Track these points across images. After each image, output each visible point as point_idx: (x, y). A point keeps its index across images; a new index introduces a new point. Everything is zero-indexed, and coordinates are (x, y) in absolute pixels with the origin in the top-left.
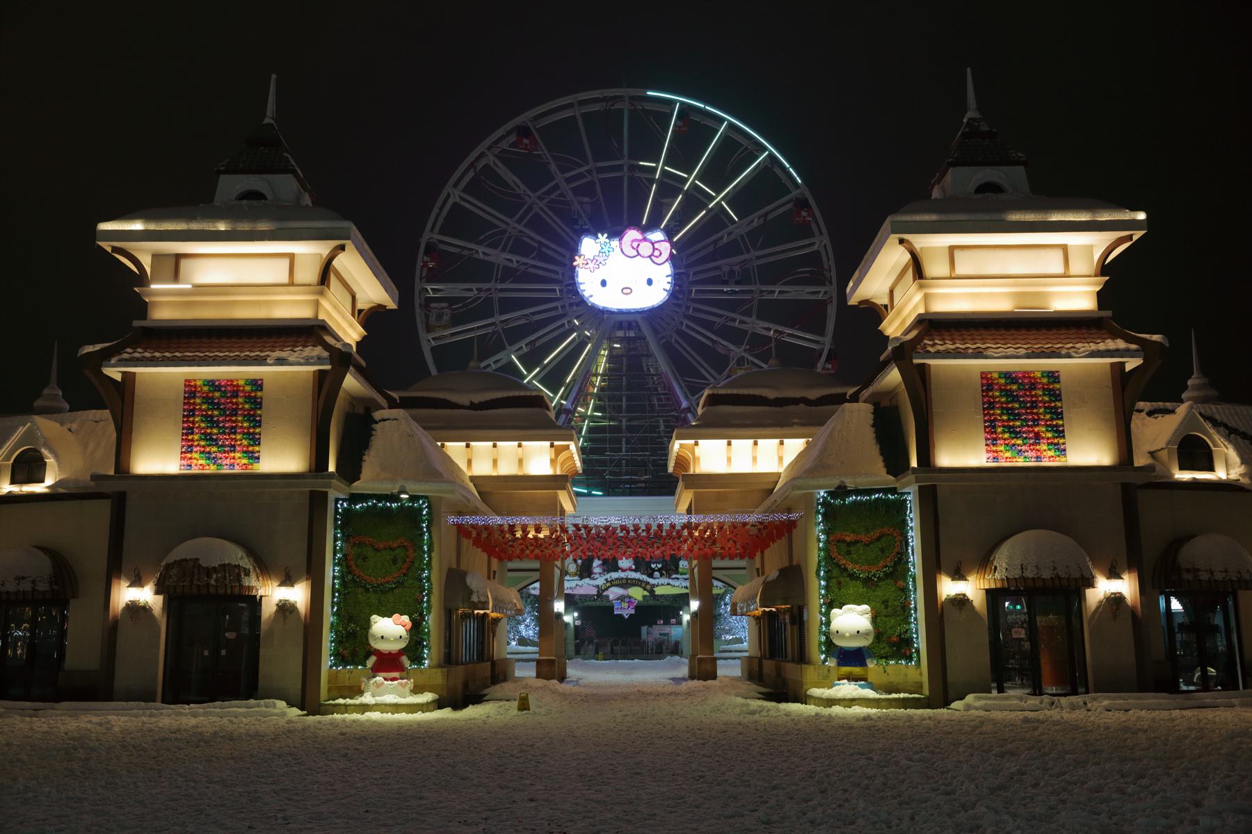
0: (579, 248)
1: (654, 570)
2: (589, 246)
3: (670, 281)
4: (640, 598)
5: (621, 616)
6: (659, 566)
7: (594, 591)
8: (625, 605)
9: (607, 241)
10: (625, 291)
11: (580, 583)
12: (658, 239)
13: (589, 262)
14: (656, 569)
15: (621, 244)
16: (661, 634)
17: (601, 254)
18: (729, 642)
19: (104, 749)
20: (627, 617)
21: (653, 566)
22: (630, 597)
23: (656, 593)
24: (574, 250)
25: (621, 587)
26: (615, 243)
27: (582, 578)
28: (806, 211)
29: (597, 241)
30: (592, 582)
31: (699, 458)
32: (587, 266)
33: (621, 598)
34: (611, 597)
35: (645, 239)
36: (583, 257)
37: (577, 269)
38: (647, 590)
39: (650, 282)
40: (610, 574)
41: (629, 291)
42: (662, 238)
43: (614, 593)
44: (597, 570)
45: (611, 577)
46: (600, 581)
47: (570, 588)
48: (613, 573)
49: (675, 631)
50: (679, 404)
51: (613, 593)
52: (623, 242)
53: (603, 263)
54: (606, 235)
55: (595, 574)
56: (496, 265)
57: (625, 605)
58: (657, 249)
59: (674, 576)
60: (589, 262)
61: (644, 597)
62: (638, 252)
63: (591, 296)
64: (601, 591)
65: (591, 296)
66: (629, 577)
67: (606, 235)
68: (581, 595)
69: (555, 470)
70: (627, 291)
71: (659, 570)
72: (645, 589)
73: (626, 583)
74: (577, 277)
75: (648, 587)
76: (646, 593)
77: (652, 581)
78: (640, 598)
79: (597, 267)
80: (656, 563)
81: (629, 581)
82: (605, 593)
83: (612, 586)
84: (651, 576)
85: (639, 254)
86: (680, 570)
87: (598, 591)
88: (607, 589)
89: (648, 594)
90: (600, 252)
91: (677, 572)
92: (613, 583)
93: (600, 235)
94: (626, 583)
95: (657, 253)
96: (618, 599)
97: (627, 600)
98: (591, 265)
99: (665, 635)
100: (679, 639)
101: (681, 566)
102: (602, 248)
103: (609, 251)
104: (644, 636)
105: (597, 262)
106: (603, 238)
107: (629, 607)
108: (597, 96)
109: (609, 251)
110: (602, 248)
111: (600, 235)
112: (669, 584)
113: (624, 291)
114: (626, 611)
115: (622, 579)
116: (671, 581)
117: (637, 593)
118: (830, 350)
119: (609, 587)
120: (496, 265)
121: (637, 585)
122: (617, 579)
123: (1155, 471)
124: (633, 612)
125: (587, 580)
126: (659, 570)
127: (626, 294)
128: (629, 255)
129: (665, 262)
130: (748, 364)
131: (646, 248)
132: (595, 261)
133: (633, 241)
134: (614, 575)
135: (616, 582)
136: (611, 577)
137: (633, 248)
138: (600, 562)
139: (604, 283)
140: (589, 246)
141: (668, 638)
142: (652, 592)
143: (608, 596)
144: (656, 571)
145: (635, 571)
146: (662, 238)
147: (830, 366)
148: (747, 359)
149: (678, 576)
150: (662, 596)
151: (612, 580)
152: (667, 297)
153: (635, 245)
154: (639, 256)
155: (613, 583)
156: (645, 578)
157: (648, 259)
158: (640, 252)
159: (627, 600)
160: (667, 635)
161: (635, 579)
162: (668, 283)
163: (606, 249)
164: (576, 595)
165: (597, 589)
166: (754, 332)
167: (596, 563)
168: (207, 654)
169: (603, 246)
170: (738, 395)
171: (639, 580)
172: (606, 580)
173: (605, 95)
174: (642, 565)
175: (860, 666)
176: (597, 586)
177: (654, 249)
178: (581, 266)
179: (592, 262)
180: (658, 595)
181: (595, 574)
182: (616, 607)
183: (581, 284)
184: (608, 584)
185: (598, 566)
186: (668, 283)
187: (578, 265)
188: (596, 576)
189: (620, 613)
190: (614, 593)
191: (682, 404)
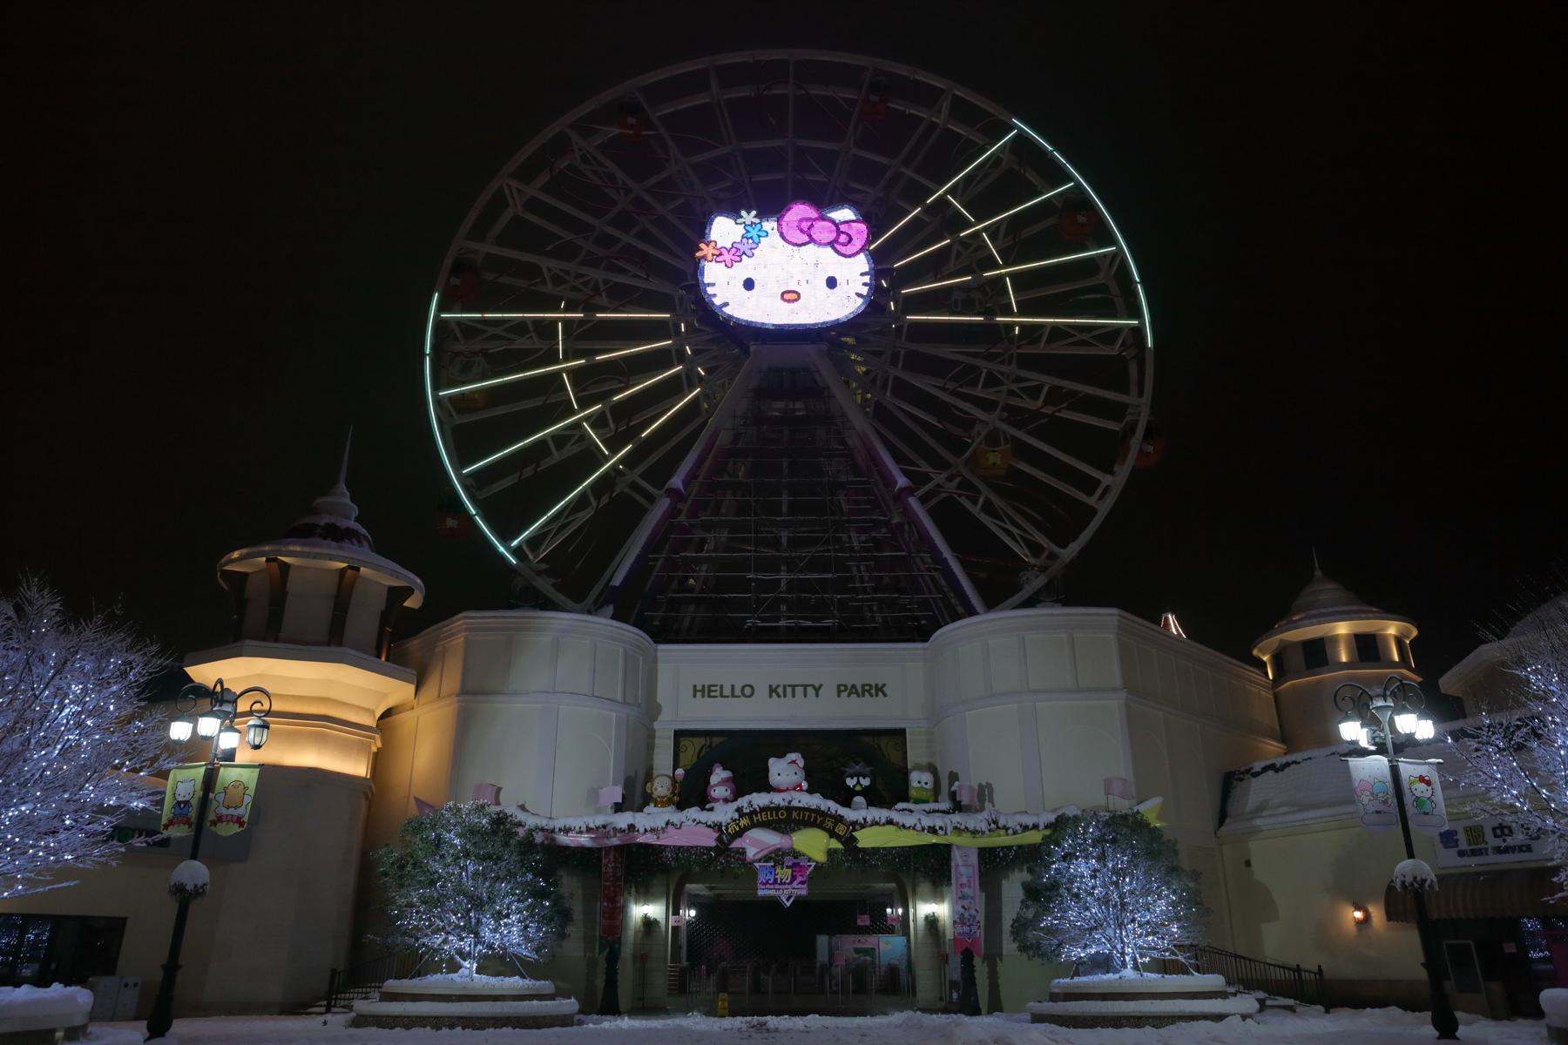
0: (707, 231)
1: (852, 793)
2: (724, 230)
3: (865, 293)
4: (821, 857)
5: (774, 903)
6: (866, 782)
7: (709, 839)
8: (784, 873)
9: (757, 221)
10: (787, 296)
11: (677, 817)
12: (846, 219)
13: (724, 251)
14: (858, 788)
15: (779, 225)
16: (858, 951)
17: (745, 240)
18: (1079, 968)
20: (788, 904)
21: (851, 782)
22: (796, 854)
23: (860, 845)
24: (701, 230)
25: (775, 829)
26: (770, 225)
27: (681, 807)
28: (1083, 216)
29: (739, 221)
30: (704, 816)
32: (720, 259)
33: (776, 857)
34: (751, 853)
35: (823, 218)
36: (713, 244)
37: (703, 263)
38: (838, 837)
39: (832, 283)
40: (747, 798)
41: (792, 296)
42: (853, 217)
44: (719, 792)
45: (750, 804)
46: (724, 814)
47: (653, 830)
48: (755, 794)
49: (887, 943)
50: (889, 481)
51: (755, 843)
52: (784, 224)
53: (749, 253)
54: (754, 213)
55: (716, 800)
57: (784, 873)
58: (843, 233)
59: (900, 805)
60: (724, 251)
61: (831, 853)
62: (810, 236)
63: (726, 304)
64: (726, 837)
65: (726, 304)
66: (795, 804)
67: (754, 213)
68: (679, 849)
70: (791, 296)
71: (865, 792)
72: (832, 834)
73: (787, 820)
74: (703, 275)
75: (841, 829)
77: (849, 814)
78: (821, 857)
79: (739, 259)
80: (858, 776)
81: (794, 814)
82: (736, 844)
83: (753, 825)
84: (847, 803)
85: (812, 240)
86: (913, 793)
87: (719, 839)
88: (740, 833)
89: (839, 846)
90: (743, 237)
91: (906, 799)
92: (758, 819)
93: (743, 213)
94: (787, 820)
95: (843, 238)
96: (767, 859)
97: (789, 861)
98: (727, 256)
99: (866, 952)
100: (896, 962)
101: (914, 784)
102: (748, 232)
103: (759, 236)
104: (822, 954)
105: (737, 253)
106: (749, 217)
107: (794, 878)
108: (744, 60)
109: (759, 236)
110: (748, 232)
111: (743, 213)
112: (890, 822)
113: (786, 296)
114: (786, 890)
115: (778, 808)
116: (895, 816)
117: (813, 844)
118: (1149, 423)
119: (746, 829)
121: (821, 827)
122: (763, 809)
125: (694, 813)
126: (865, 792)
127: (789, 301)
128: (794, 241)
129: (857, 253)
130: (1005, 444)
131: (823, 231)
132: (734, 250)
133: (801, 220)
134: (759, 799)
135: (763, 817)
136: (750, 804)
137: (802, 231)
138: (726, 774)
139: (749, 284)
140: (724, 230)
141: (873, 957)
142: (850, 842)
143: (743, 852)
144: (859, 793)
145: (810, 791)
146: (853, 217)
147: (1150, 449)
148: (1004, 433)
149: (910, 806)
150: (875, 851)
151: (754, 812)
152: (863, 308)
153: (805, 225)
154: (811, 246)
155: (758, 819)
156: (831, 806)
157: (829, 250)
158: (814, 236)
159: (789, 861)
160: (870, 952)
161: (808, 809)
162: (865, 284)
163: (754, 233)
164: (666, 847)
165: (717, 835)
166: (1008, 404)
167: (719, 775)
168: (1507, 950)
169: (749, 228)
170: (961, 588)
171: (818, 811)
172: (739, 810)
173: (758, 58)
174: (824, 778)
175: (1054, 993)
176: (717, 827)
177: (839, 232)
178: (710, 257)
179: (729, 252)
180: (864, 850)
181: (716, 800)
182: (761, 878)
183: (709, 285)
184: (744, 822)
185: (723, 782)
186: (865, 284)
187: (704, 257)
188: (717, 806)
189: (772, 892)
191: (896, 483)
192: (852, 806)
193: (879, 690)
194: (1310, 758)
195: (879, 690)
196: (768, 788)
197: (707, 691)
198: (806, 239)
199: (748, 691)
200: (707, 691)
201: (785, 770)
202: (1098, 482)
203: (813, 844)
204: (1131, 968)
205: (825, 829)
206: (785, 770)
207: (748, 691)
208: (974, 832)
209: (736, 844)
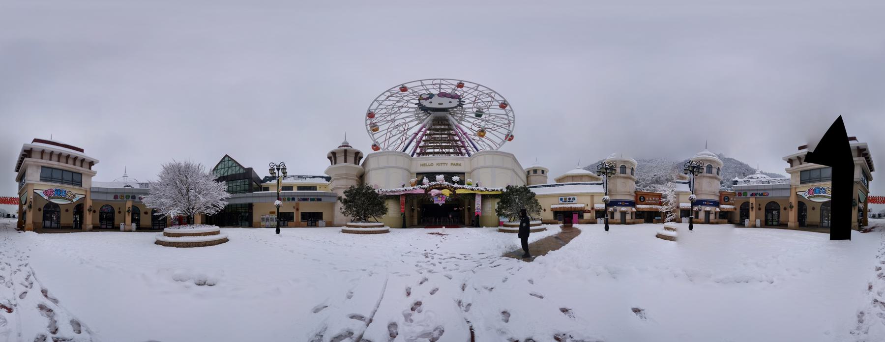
5: (438, 204)
7: (423, 192)
8: (440, 199)
19: (469, 119)
22: (442, 194)
31: (18, 194)
33: (438, 195)
34: (432, 194)
43: (434, 192)
56: (478, 113)
61: (450, 194)
64: (427, 190)
69: (856, 179)
72: (451, 190)
73: (440, 188)
76: (451, 193)
82: (429, 193)
88: (430, 190)
92: (431, 188)
94: (440, 188)
96: (436, 196)
112: (463, 188)
114: (440, 202)
115: (438, 185)
119: (432, 189)
120: (478, 113)
121: (448, 189)
123: (867, 225)
124: (444, 203)
134: (434, 183)
142: (454, 192)
143: (431, 194)
159: (441, 196)
184: (431, 188)
190: (434, 192)
192: (253, 225)
193: (460, 165)
194: (348, 271)
195: (460, 165)
196: (436, 181)
197: (424, 165)
198: (423, 81)
199: (432, 165)
200: (424, 165)
201: (440, 178)
202: (720, 218)
203: (446, 192)
204: (505, 211)
205: (449, 189)
206: (440, 178)
207: (432, 165)
208: (481, 191)
209: (429, 193)
